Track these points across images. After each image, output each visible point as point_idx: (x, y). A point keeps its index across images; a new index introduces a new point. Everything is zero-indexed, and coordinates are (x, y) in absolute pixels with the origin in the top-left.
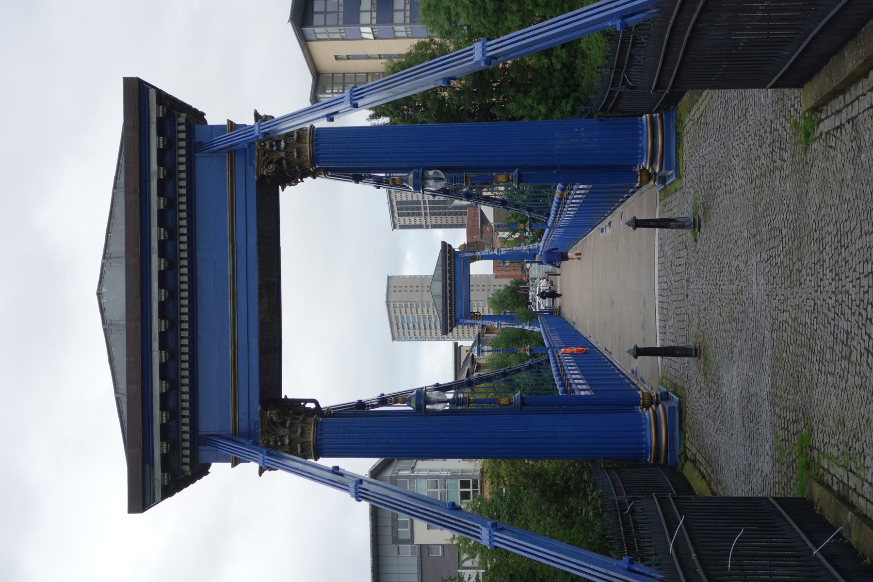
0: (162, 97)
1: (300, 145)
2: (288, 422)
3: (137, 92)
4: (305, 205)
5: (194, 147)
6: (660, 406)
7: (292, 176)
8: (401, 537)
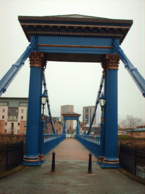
0: (127, 31)
1: (114, 66)
2: (40, 59)
3: (129, 23)
4: (94, 71)
5: (114, 38)
6: (39, 160)
7: (103, 66)
8: (21, 104)
